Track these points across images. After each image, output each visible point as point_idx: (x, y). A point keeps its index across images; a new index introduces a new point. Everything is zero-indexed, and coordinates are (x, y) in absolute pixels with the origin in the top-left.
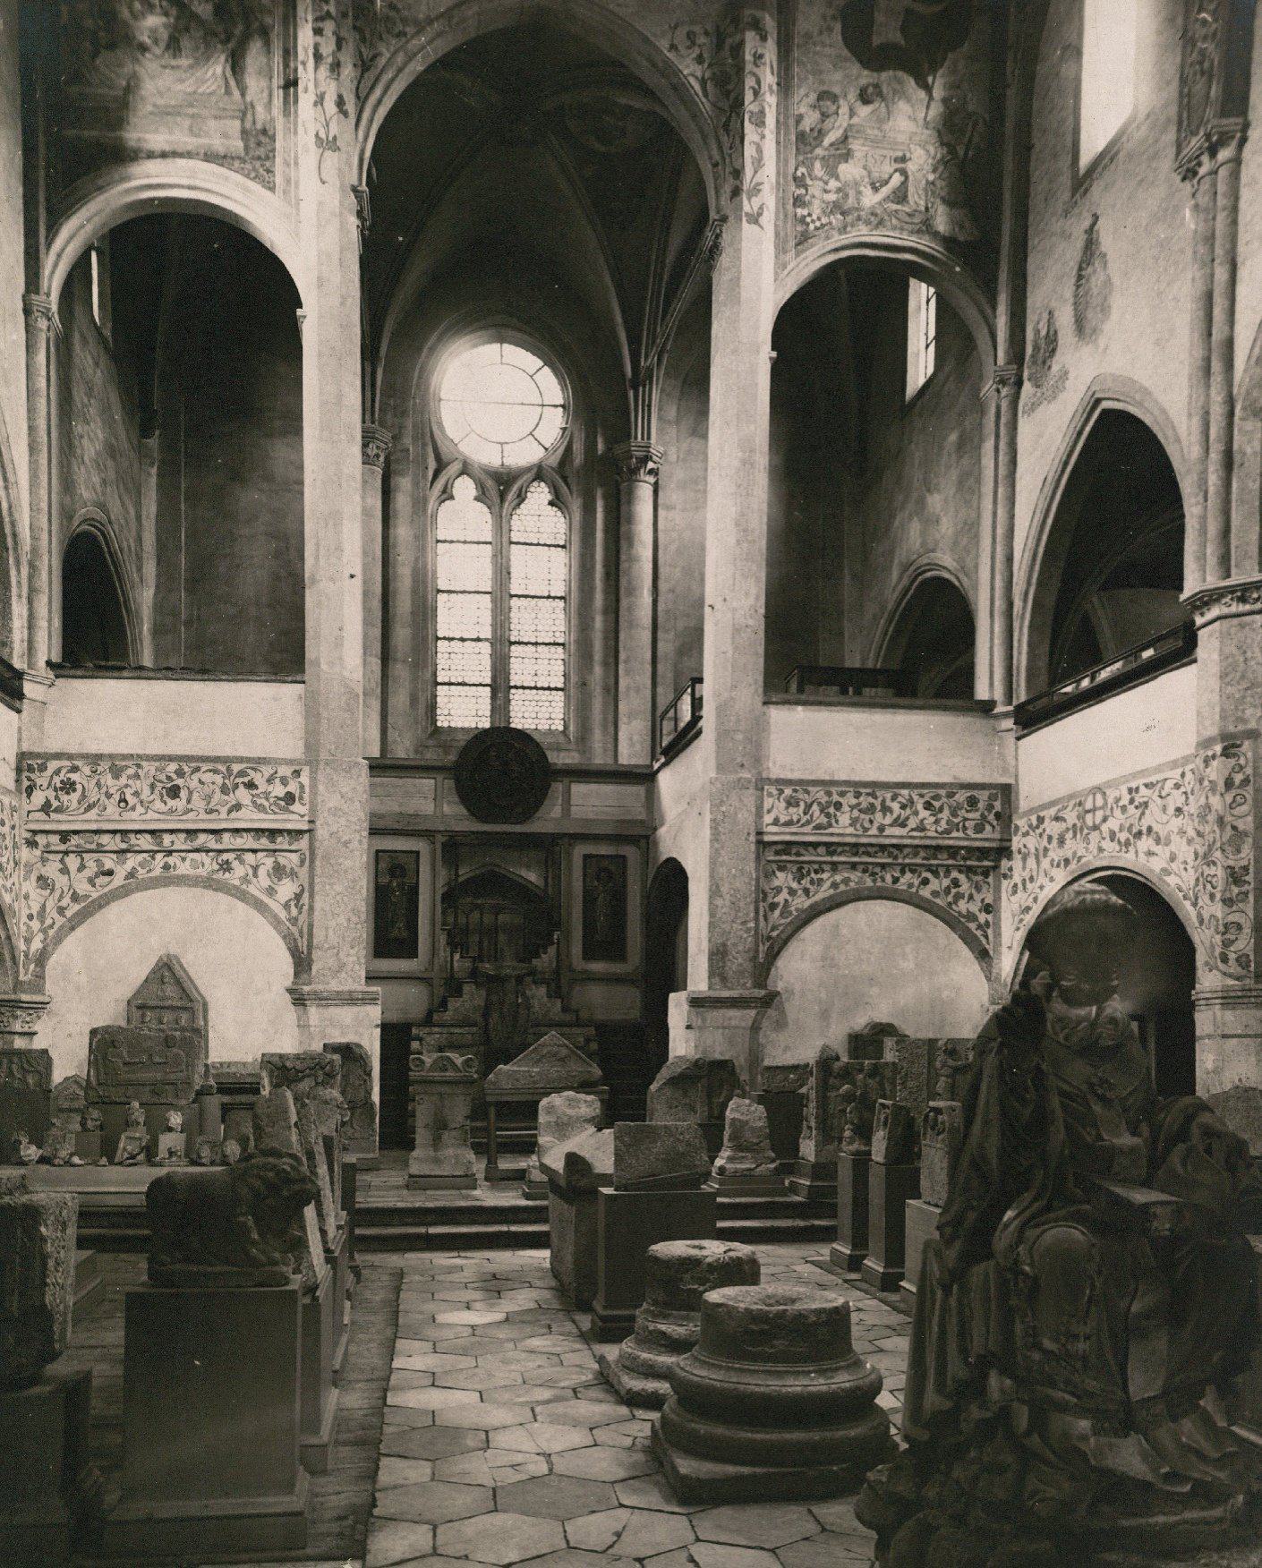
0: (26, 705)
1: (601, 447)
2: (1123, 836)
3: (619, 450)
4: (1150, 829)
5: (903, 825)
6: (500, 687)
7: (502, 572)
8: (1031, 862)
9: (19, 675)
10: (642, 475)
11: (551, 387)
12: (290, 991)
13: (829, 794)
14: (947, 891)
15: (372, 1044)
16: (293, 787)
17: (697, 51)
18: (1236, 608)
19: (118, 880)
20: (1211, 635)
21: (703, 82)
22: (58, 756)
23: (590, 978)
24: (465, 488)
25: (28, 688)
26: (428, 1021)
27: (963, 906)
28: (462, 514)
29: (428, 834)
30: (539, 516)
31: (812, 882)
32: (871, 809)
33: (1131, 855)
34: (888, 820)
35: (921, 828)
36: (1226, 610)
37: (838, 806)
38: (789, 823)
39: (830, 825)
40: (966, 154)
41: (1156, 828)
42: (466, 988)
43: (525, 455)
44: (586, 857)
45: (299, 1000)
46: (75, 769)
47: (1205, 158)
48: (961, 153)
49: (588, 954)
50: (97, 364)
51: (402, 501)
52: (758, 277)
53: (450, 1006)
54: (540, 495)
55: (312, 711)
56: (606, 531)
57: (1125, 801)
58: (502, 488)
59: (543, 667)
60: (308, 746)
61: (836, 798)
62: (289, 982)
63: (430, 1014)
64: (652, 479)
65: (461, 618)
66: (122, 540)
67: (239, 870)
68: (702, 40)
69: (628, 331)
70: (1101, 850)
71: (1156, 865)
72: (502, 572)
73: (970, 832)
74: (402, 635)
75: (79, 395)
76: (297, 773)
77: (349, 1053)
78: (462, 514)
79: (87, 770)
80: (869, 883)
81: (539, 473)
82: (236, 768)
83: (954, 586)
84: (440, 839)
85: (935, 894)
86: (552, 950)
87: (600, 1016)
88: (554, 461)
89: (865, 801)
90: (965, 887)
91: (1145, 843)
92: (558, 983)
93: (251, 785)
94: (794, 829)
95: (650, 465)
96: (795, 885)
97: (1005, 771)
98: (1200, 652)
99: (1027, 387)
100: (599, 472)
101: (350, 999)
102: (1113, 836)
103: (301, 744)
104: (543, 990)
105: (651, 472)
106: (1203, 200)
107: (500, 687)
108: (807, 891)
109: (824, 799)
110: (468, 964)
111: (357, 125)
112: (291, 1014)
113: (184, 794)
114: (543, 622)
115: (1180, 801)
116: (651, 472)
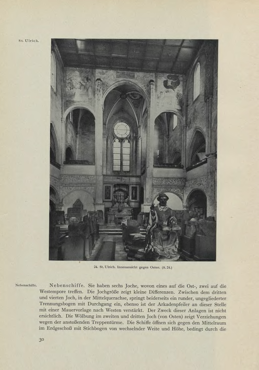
0: (61, 169)
1: (134, 135)
2: (199, 184)
3: (137, 136)
4: (202, 184)
5: (171, 183)
6: (121, 165)
7: (121, 150)
8: (188, 188)
9: (60, 165)
10: (140, 139)
11: (128, 128)
12: (93, 203)
13: (162, 179)
14: (177, 191)
15: (103, 210)
16: (93, 178)
17: (145, 87)
18: (212, 156)
19: (72, 190)
20: (209, 159)
21: (146, 91)
22: (64, 175)
23: (132, 202)
24: (117, 140)
25: (61, 167)
26: (112, 207)
27: (179, 193)
28: (117, 143)
29: (112, 184)
30: (126, 144)
31: (159, 190)
32: (167, 181)
33: (200, 187)
34: (169, 182)
35: (174, 183)
36: (211, 156)
37: (163, 181)
38: (156, 183)
39: (162, 183)
40: (180, 98)
41: (203, 184)
42: (117, 203)
43: (125, 136)
44: (132, 187)
45: (94, 205)
46: (67, 176)
47: (208, 100)
48: (179, 98)
49: (132, 199)
50: (70, 127)
51: (109, 142)
52: (155, 111)
53: (114, 206)
54: (126, 141)
55: (96, 168)
56: (135, 146)
57: (199, 180)
58: (121, 140)
59: (127, 163)
60: (95, 174)
61: (163, 180)
62: (93, 202)
63: (112, 206)
64: (141, 139)
65: (117, 157)
66: (73, 148)
67: (87, 189)
68: (146, 86)
69: (138, 120)
70: (196, 186)
71: (203, 188)
72: (121, 150)
73: (180, 184)
74: (109, 159)
75: (68, 130)
76: (94, 177)
77: (101, 211)
78: (117, 143)
79: (68, 176)
80: (167, 190)
81: (126, 138)
82: (87, 176)
83: (201, 132)
84: (114, 185)
85: (176, 192)
86: (127, 198)
87: (133, 207)
88: (128, 137)
89: (166, 180)
90: (179, 191)
91: (202, 185)
92: (128, 203)
93: (88, 178)
94: (157, 184)
95: (141, 137)
96: (157, 191)
97: (100, 228)
98: (208, 162)
99: (188, 128)
100: (134, 138)
101: (101, 204)
102: (198, 185)
103: (95, 173)
104: (126, 204)
105: (141, 138)
106: (207, 105)
107: (121, 165)
108: (159, 191)
109: (161, 180)
110: (117, 200)
111: (102, 97)
112: (93, 206)
113: (80, 179)
114: (126, 157)
115: (206, 180)
116: (141, 138)
